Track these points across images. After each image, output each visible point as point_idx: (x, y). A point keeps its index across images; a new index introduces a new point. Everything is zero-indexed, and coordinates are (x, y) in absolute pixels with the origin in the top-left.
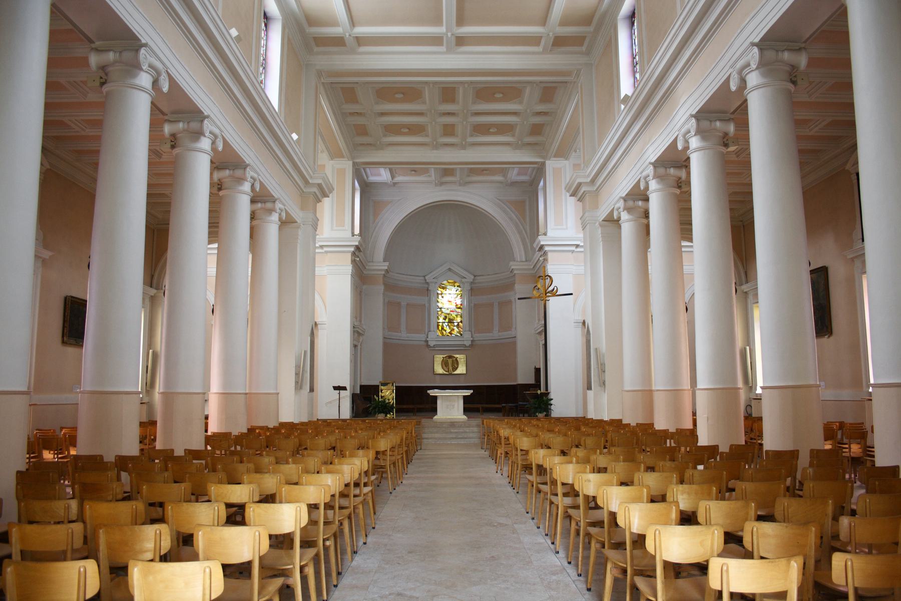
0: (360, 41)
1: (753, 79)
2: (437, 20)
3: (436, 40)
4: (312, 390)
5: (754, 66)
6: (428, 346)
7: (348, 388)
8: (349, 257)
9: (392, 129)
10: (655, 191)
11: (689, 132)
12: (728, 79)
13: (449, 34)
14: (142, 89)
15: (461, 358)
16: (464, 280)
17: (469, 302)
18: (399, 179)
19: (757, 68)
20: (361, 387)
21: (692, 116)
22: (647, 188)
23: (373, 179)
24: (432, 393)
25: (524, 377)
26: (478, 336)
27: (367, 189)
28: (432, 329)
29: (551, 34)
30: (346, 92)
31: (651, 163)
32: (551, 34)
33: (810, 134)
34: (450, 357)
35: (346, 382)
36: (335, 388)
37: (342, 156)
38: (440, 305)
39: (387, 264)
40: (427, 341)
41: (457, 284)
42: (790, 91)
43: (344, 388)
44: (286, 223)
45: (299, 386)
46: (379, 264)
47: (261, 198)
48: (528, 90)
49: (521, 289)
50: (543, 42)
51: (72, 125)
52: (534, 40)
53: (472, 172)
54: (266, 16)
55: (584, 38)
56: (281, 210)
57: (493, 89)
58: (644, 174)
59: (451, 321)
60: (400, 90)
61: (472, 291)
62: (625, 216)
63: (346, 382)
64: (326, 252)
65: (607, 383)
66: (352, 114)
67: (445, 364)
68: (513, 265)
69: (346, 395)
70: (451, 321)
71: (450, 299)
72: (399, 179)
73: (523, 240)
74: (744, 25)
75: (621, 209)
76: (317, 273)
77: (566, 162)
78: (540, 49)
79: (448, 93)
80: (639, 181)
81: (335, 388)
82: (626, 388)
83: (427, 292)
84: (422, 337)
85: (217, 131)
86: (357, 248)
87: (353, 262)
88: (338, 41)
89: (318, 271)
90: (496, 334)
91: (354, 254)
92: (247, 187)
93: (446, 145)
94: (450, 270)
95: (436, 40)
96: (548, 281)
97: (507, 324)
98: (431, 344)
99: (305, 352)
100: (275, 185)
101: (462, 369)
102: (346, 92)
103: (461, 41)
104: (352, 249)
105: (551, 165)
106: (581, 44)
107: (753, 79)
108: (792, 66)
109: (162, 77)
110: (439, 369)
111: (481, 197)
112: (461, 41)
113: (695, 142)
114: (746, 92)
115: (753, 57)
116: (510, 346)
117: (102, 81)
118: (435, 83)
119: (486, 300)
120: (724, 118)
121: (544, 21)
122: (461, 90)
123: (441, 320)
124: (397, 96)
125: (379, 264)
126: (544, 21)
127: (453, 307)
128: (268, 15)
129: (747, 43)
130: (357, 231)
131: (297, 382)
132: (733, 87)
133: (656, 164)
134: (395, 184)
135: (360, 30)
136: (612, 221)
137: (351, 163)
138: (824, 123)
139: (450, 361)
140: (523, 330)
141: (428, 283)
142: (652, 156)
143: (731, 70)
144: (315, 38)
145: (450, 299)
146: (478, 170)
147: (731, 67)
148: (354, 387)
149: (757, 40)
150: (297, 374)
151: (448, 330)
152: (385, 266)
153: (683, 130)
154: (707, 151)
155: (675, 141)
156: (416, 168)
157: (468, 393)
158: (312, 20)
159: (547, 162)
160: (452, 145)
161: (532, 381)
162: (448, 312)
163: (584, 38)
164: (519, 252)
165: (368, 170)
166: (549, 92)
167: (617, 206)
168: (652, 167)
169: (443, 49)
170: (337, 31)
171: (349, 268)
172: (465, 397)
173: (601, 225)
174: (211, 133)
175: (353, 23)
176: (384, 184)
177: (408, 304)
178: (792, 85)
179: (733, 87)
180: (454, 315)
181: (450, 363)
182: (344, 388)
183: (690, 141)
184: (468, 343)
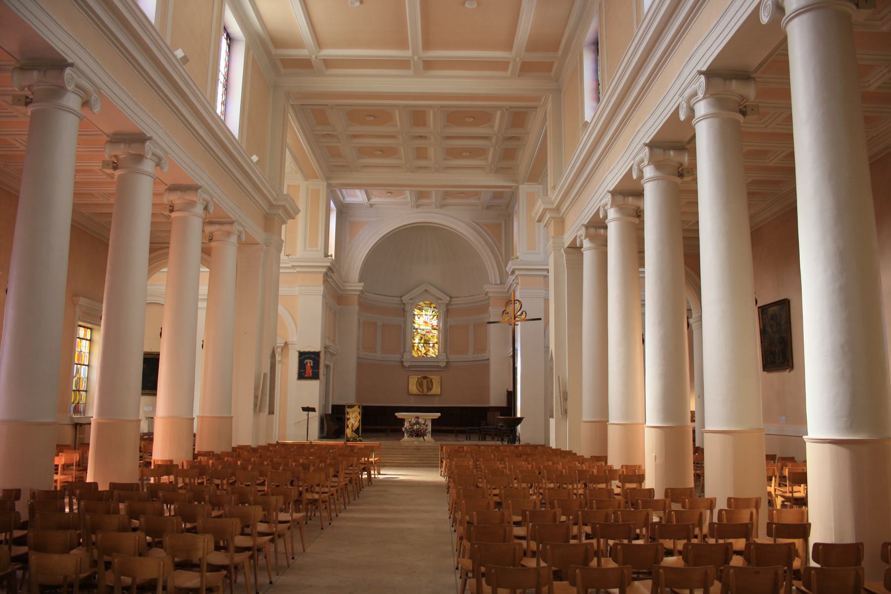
0: (329, 63)
1: (702, 108)
2: (402, 43)
3: (403, 64)
4: (271, 412)
5: (701, 95)
6: (403, 366)
7: (317, 409)
8: (321, 277)
9: (363, 152)
10: (613, 220)
11: (642, 161)
12: (677, 109)
13: (416, 58)
14: (70, 110)
15: (436, 379)
16: (440, 302)
17: (445, 323)
18: (374, 200)
19: (704, 98)
20: (334, 407)
21: (646, 145)
22: (606, 217)
23: (349, 200)
24: (399, 415)
25: (496, 399)
26: (453, 357)
27: (344, 211)
28: (407, 349)
29: (518, 59)
30: (317, 114)
31: (609, 192)
32: (518, 59)
33: (771, 164)
34: (425, 378)
35: (315, 403)
36: (304, 409)
37: (317, 178)
38: (416, 326)
39: (362, 284)
40: (402, 362)
41: (433, 306)
42: (738, 122)
43: (313, 410)
44: (246, 244)
45: (257, 408)
46: (354, 285)
47: (215, 220)
48: (499, 114)
49: (494, 312)
50: (511, 66)
51: (17, 144)
52: (500, 65)
53: (447, 194)
54: (229, 37)
55: (508, 63)
56: (240, 232)
57: (462, 115)
58: (603, 202)
59: (426, 342)
60: (369, 113)
61: (447, 313)
62: (587, 244)
63: (315, 403)
64: (299, 272)
65: (569, 412)
66: (324, 136)
67: (420, 384)
68: (488, 288)
69: (315, 417)
70: (426, 342)
71: (425, 321)
72: (374, 200)
73: (498, 262)
74: (691, 53)
75: (583, 237)
76: (281, 293)
77: (540, 186)
78: (509, 73)
79: (418, 117)
80: (599, 210)
81: (304, 409)
82: (584, 419)
83: (404, 314)
84: (397, 357)
85: (159, 152)
86: (330, 269)
87: (325, 281)
88: (305, 64)
89: (283, 290)
90: (471, 356)
91: (326, 274)
92: (199, 209)
93: (420, 168)
94: (426, 291)
95: (403, 64)
96: (517, 305)
97: (482, 346)
98: (406, 364)
99: (265, 375)
100: (229, 205)
101: (436, 390)
102: (317, 114)
103: (429, 65)
104: (324, 270)
105: (524, 189)
106: (506, 69)
107: (702, 108)
108: (742, 96)
109: (93, 98)
110: (413, 389)
111: (455, 220)
112: (429, 65)
113: (649, 172)
114: (694, 122)
115: (700, 86)
116: (483, 367)
117: (28, 100)
118: (406, 106)
119: (459, 324)
120: (673, 148)
121: (509, 46)
122: (431, 112)
123: (417, 340)
124: (367, 118)
125: (354, 285)
126: (509, 46)
127: (429, 328)
128: (231, 36)
129: (695, 71)
130: (332, 251)
131: (255, 405)
132: (682, 117)
133: (614, 193)
134: (371, 205)
135: (328, 52)
136: (575, 249)
137: (325, 183)
138: (784, 154)
139: (425, 381)
140: (496, 353)
141: (404, 304)
142: (610, 185)
143: (681, 99)
144: (282, 61)
145: (425, 321)
146: (449, 195)
147: (681, 95)
148: (325, 406)
149: (704, 69)
150: (256, 397)
151: (424, 351)
152: (360, 286)
153: (638, 159)
154: (660, 181)
155: (630, 171)
156: (391, 189)
157: (437, 415)
158: (278, 42)
159: (521, 187)
160: (426, 168)
161: (503, 403)
162: (424, 333)
163: (508, 63)
164: (493, 275)
165: (344, 191)
166: (519, 117)
167: (579, 233)
168: (610, 196)
169: (410, 72)
170: (303, 53)
171: (321, 289)
172: (433, 421)
173: (566, 252)
174: (153, 154)
175: (319, 44)
176: (360, 205)
177: (384, 325)
178: (741, 116)
179: (682, 117)
180: (429, 336)
181: (425, 382)
182: (313, 410)
183: (644, 170)
184: (443, 364)
